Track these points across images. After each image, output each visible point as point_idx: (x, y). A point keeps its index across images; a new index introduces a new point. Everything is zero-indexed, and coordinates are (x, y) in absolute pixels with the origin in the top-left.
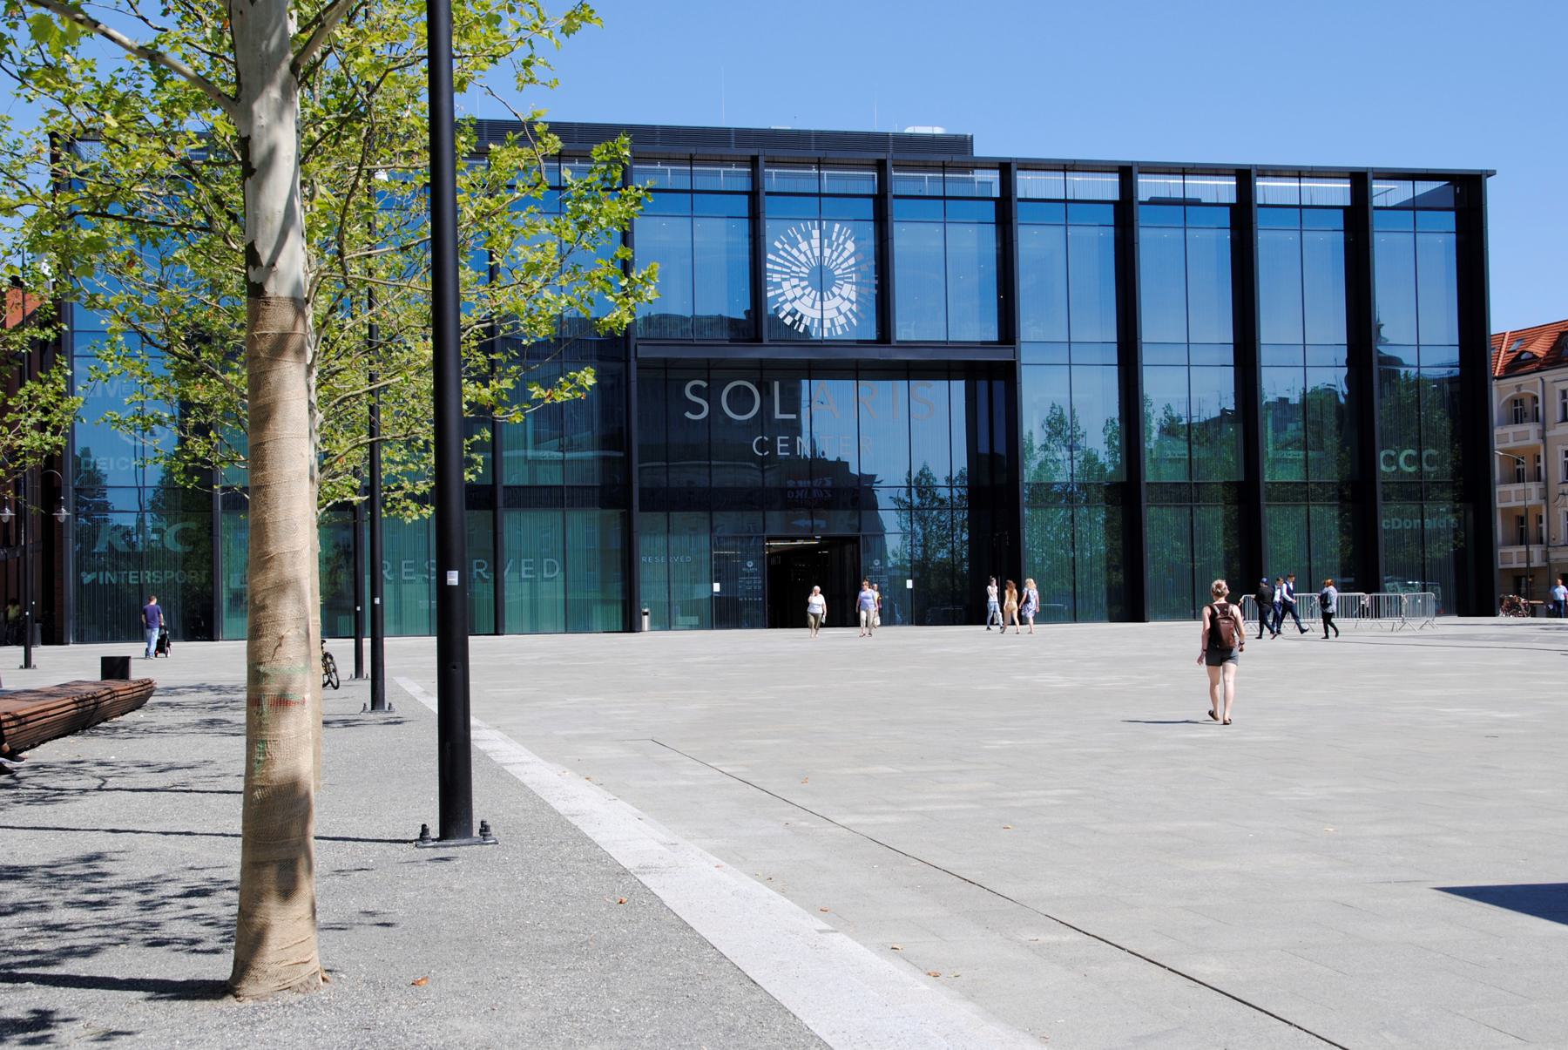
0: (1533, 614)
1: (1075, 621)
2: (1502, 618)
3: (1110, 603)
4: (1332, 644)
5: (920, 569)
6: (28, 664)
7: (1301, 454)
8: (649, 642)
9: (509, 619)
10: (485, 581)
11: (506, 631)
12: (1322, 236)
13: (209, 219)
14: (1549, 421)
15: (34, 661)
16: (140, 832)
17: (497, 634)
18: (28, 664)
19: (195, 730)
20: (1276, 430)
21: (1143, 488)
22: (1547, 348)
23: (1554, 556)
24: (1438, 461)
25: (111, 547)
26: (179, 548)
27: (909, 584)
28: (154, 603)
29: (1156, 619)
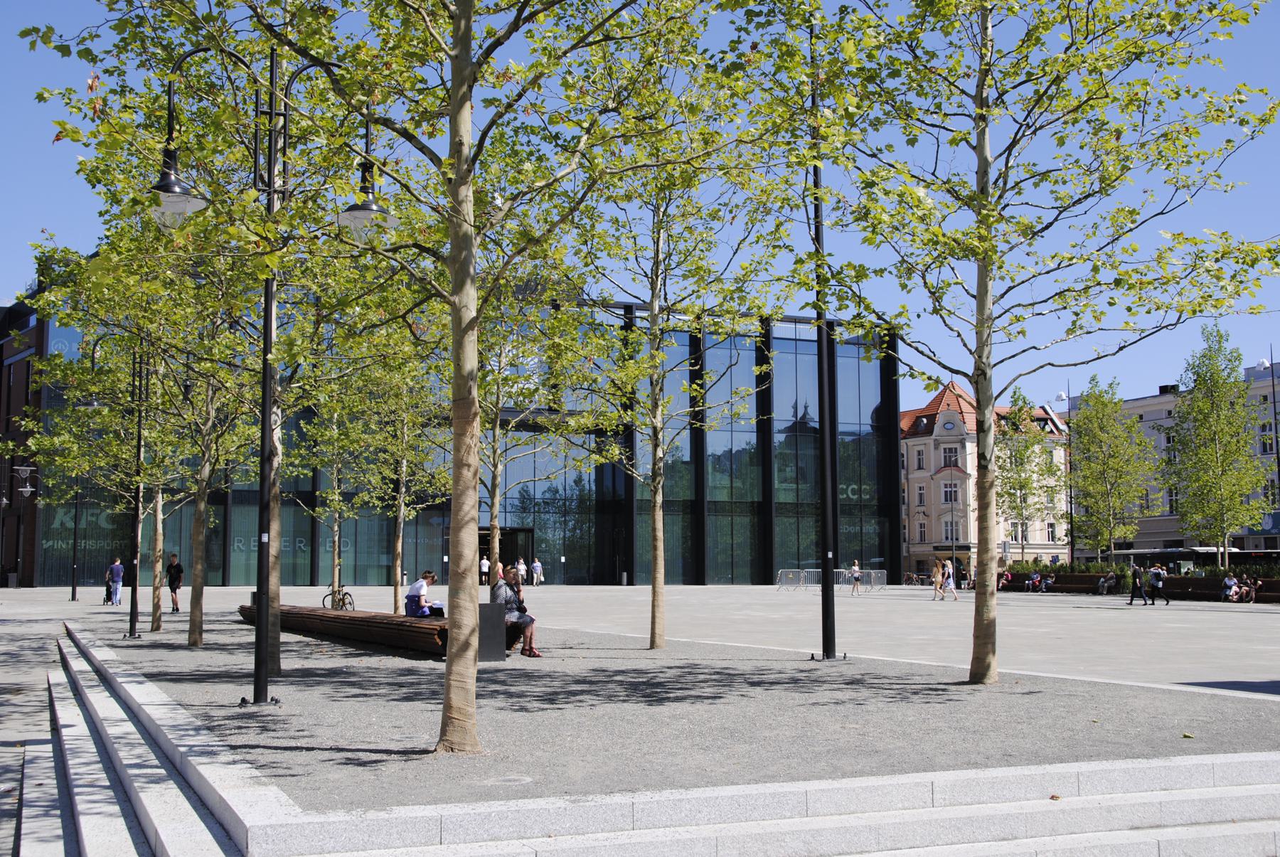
0: (922, 584)
1: (733, 583)
2: (904, 586)
3: (684, 574)
4: (938, 605)
5: (568, 548)
6: (74, 598)
7: (794, 486)
8: (903, 589)
9: (709, 572)
10: (304, 551)
11: (231, 582)
12: (807, 358)
13: (730, 88)
14: (911, 469)
15: (77, 597)
16: (313, 749)
17: (224, 585)
18: (74, 598)
19: (840, 695)
20: (780, 470)
21: (706, 504)
22: (909, 425)
23: (912, 549)
24: (868, 492)
25: (62, 524)
26: (110, 527)
27: (563, 559)
28: (118, 563)
29: (713, 583)
